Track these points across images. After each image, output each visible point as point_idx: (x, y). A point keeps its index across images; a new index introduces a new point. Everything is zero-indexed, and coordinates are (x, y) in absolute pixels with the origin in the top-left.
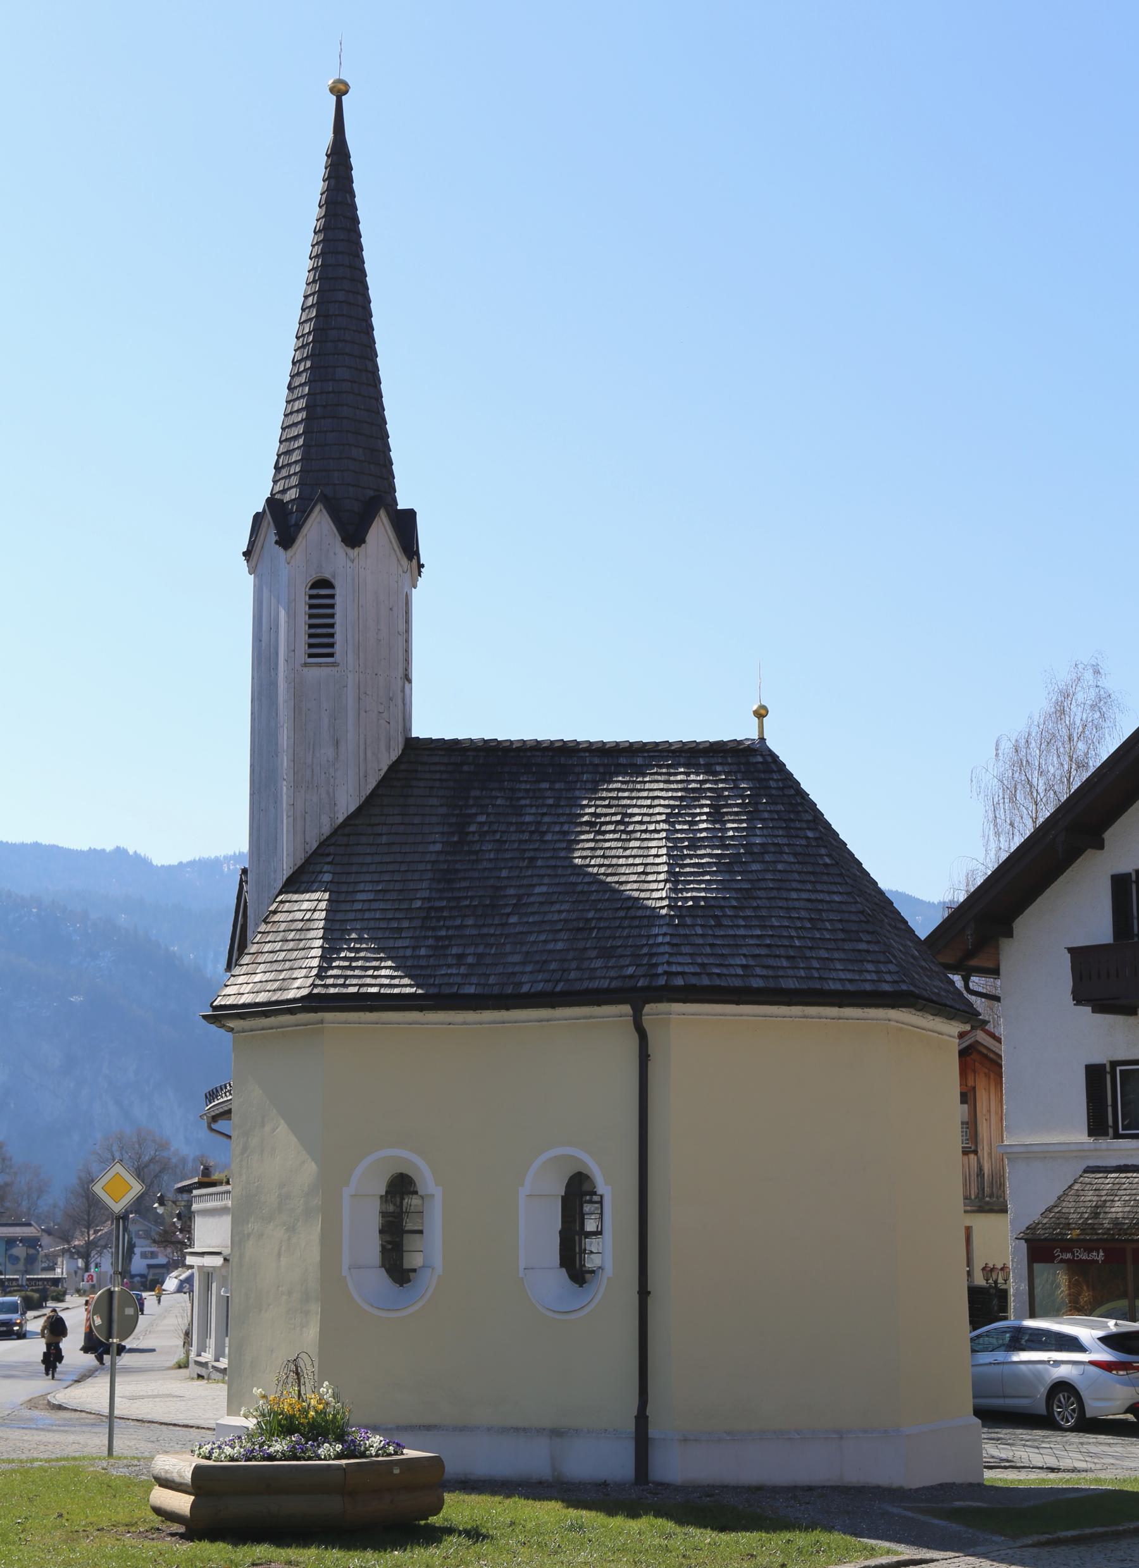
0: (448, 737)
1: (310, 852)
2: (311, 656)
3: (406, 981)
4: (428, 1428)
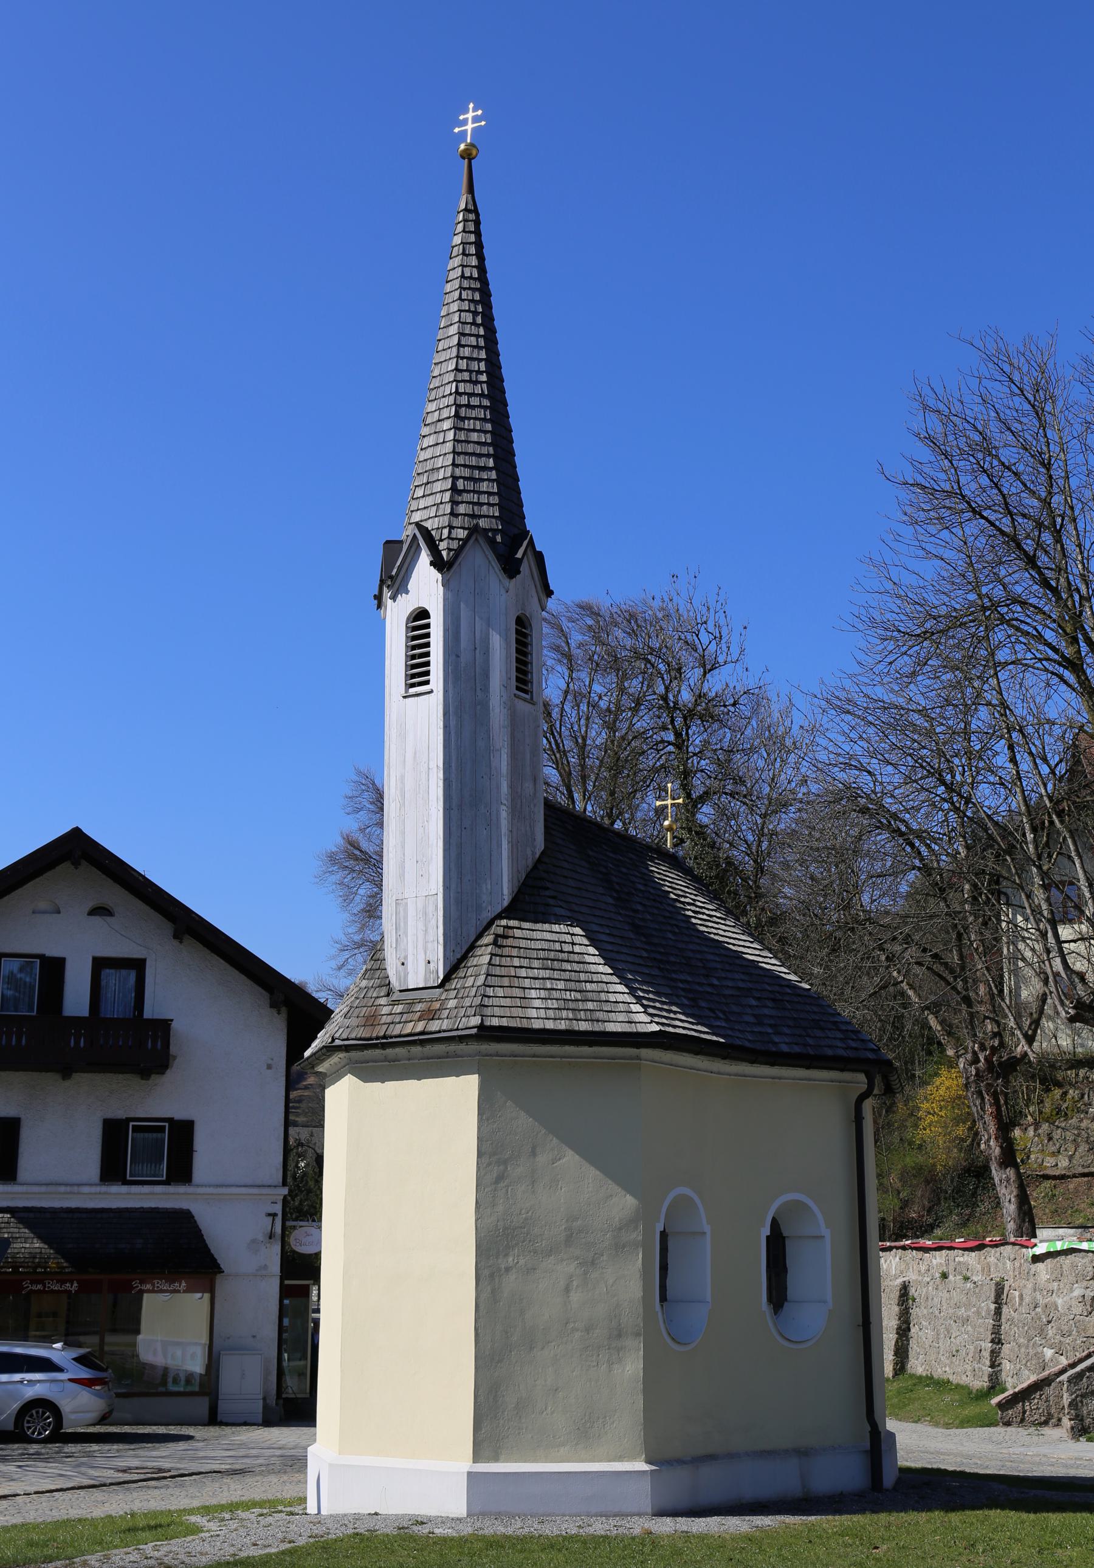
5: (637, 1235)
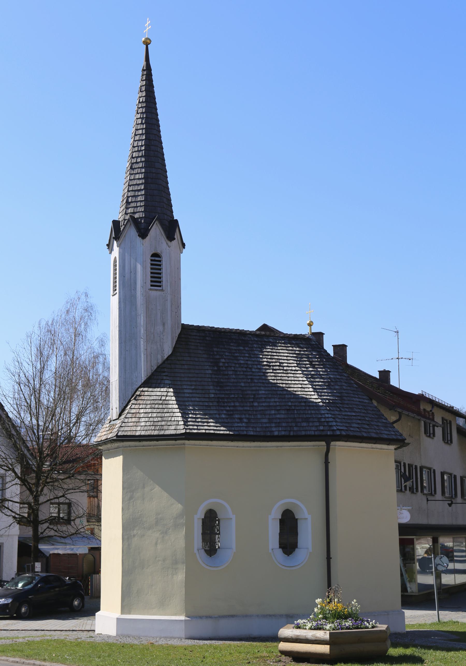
0: (195, 324)
1: (153, 370)
2: (152, 286)
3: (222, 428)
4: (233, 616)
5: (183, 521)
